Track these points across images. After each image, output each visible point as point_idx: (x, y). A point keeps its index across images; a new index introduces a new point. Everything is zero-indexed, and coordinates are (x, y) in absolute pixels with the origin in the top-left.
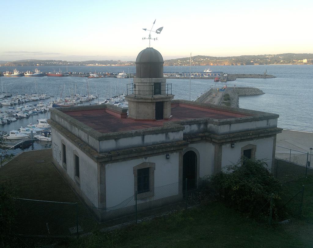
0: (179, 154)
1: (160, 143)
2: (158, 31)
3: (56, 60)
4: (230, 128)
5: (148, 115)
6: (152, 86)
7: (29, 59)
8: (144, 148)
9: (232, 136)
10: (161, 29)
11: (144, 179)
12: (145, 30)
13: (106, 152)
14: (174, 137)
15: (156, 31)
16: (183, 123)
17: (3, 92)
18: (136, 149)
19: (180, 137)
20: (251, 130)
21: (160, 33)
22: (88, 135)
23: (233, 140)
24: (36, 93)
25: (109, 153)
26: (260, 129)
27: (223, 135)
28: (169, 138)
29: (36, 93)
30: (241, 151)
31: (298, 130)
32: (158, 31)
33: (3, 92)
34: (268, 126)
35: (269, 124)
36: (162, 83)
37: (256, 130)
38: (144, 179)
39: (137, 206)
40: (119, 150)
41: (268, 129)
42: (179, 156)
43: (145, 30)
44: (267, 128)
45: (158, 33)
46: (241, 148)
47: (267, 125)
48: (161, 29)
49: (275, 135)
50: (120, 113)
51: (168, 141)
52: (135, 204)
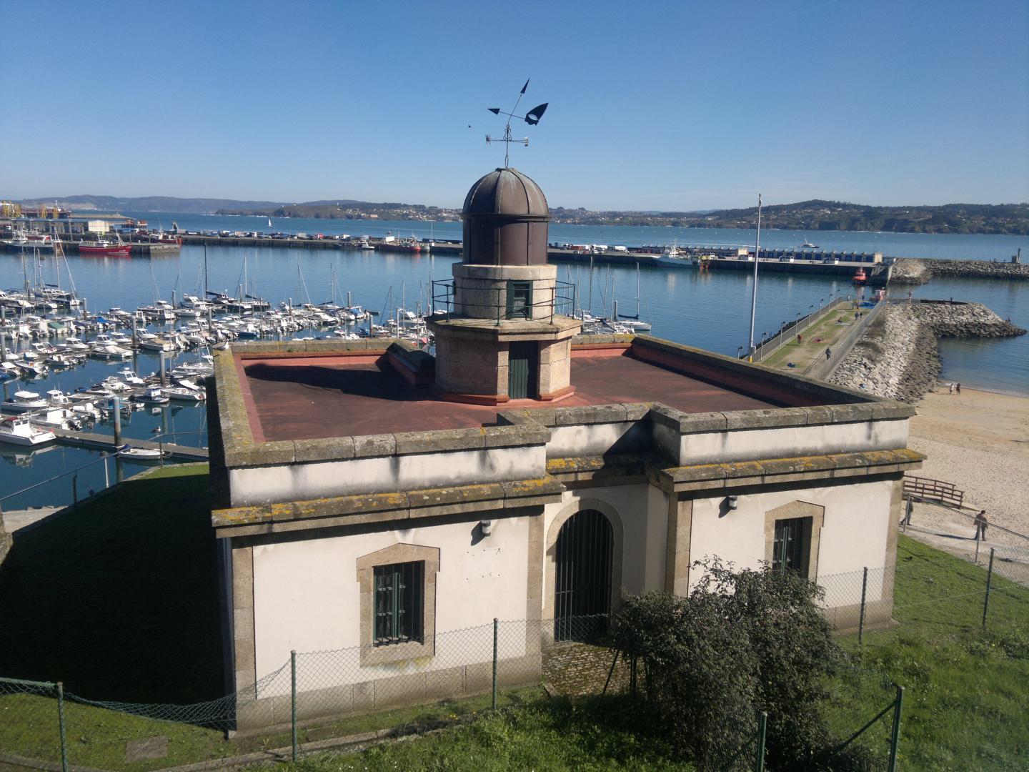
0: (530, 524)
1: (458, 481)
2: (533, 117)
3: (408, 204)
4: (723, 444)
5: (485, 381)
6: (447, 286)
7: (58, 196)
8: (395, 498)
9: (728, 468)
10: (539, 111)
11: (400, 602)
12: (496, 111)
13: (253, 504)
14: (512, 463)
15: (525, 117)
16: (562, 418)
17: (247, 296)
18: (367, 500)
19: (533, 466)
20: (804, 454)
21: (536, 122)
22: (161, 443)
23: (731, 483)
24: (332, 302)
25: (267, 508)
26: (839, 452)
27: (712, 463)
28: (492, 467)
29: (332, 302)
30: (767, 521)
31: (734, 477)
32: (533, 117)
33: (247, 296)
34: (871, 443)
35: (876, 436)
36: (535, 284)
37: (826, 454)
38: (400, 602)
39: (297, 700)
40: (303, 498)
41: (865, 454)
42: (530, 530)
43: (496, 111)
44: (865, 451)
45: (530, 122)
46: (764, 514)
47: (869, 437)
48: (539, 111)
49: (560, 494)
50: (414, 370)
51: (488, 475)
52: (289, 691)
